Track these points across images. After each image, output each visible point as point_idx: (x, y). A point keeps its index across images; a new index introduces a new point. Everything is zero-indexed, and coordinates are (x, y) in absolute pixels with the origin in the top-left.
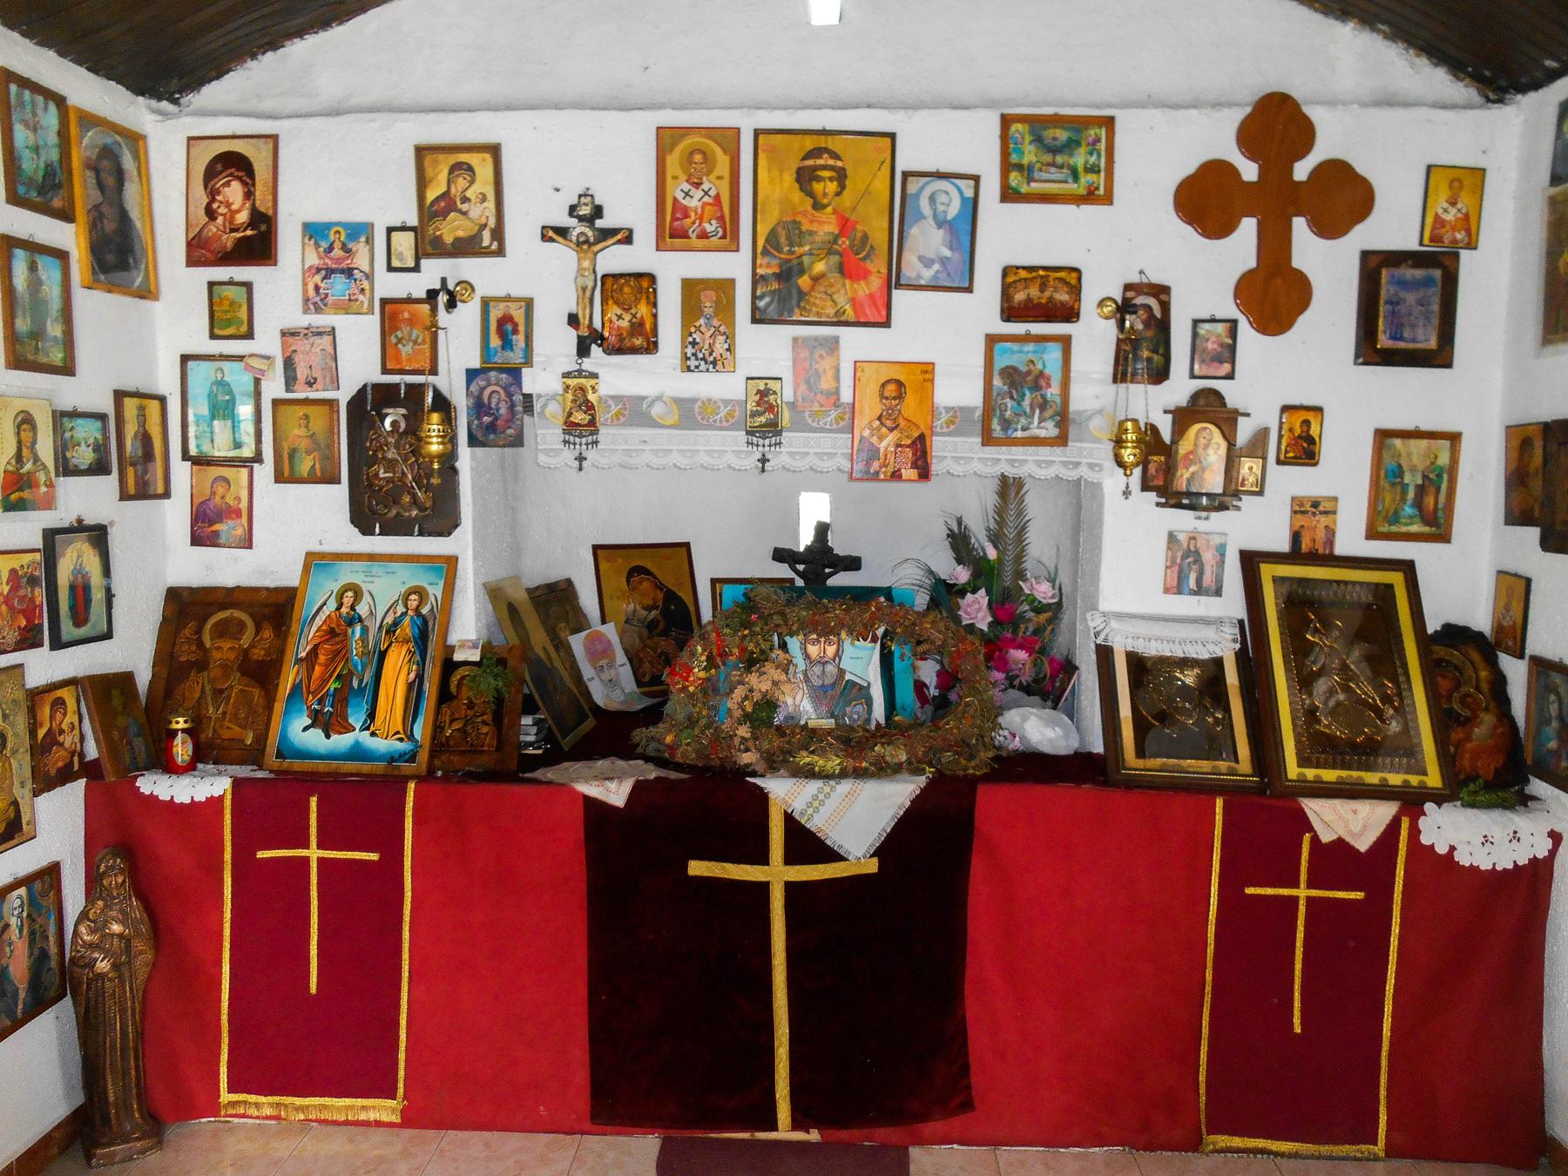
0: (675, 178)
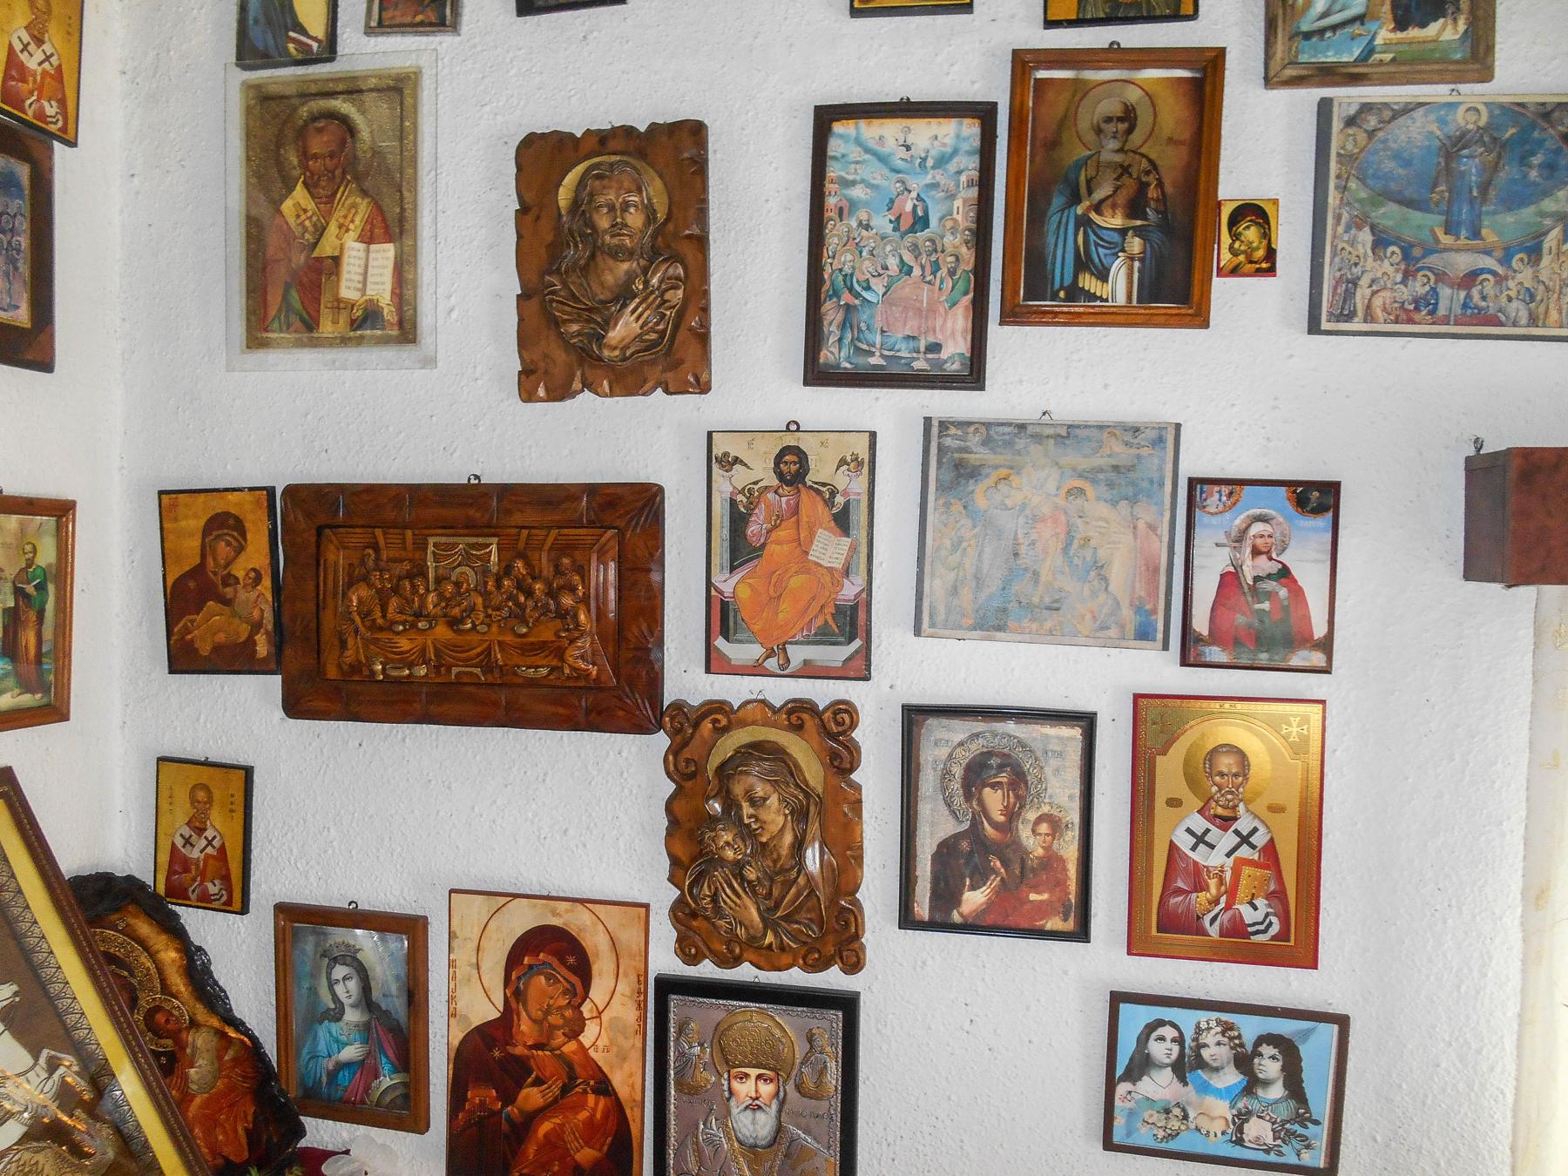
0: (1174, 803)
